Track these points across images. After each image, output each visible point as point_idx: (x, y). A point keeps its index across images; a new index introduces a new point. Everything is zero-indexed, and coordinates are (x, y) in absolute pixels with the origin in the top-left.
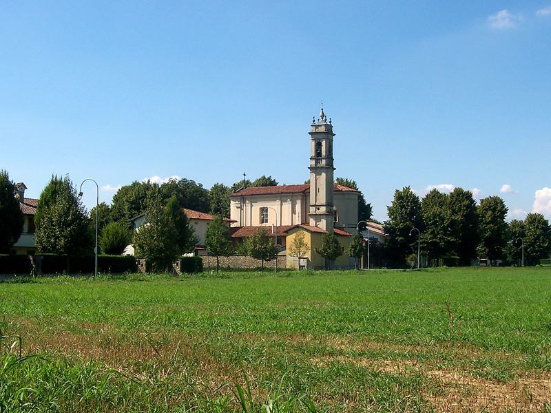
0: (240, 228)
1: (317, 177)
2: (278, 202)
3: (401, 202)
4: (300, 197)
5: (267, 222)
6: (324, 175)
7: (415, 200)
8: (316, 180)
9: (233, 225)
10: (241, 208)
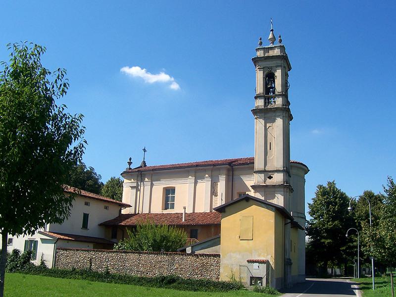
0: (135, 214)
1: (268, 125)
2: (191, 179)
3: (327, 198)
4: (225, 172)
5: (173, 207)
6: (279, 122)
7: (344, 199)
8: (266, 130)
9: (124, 211)
10: (137, 188)
